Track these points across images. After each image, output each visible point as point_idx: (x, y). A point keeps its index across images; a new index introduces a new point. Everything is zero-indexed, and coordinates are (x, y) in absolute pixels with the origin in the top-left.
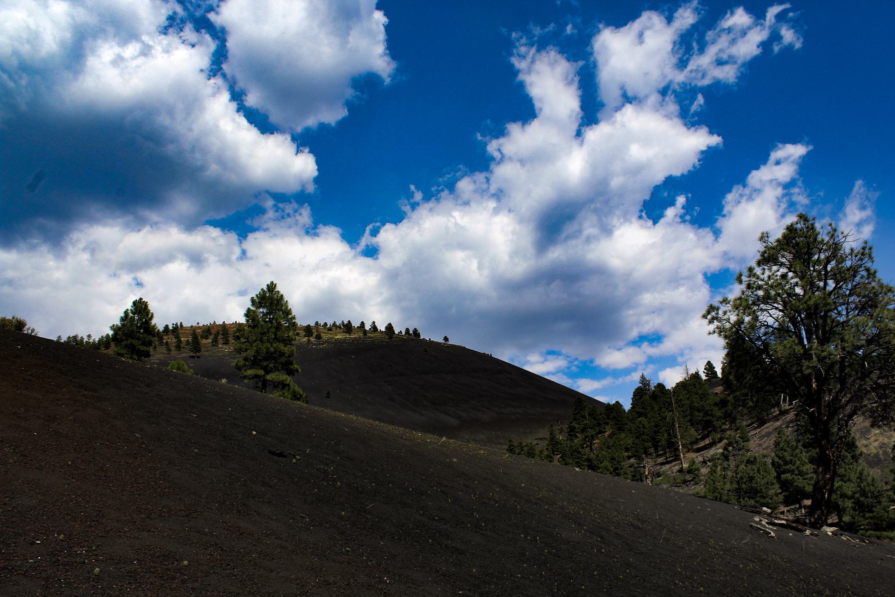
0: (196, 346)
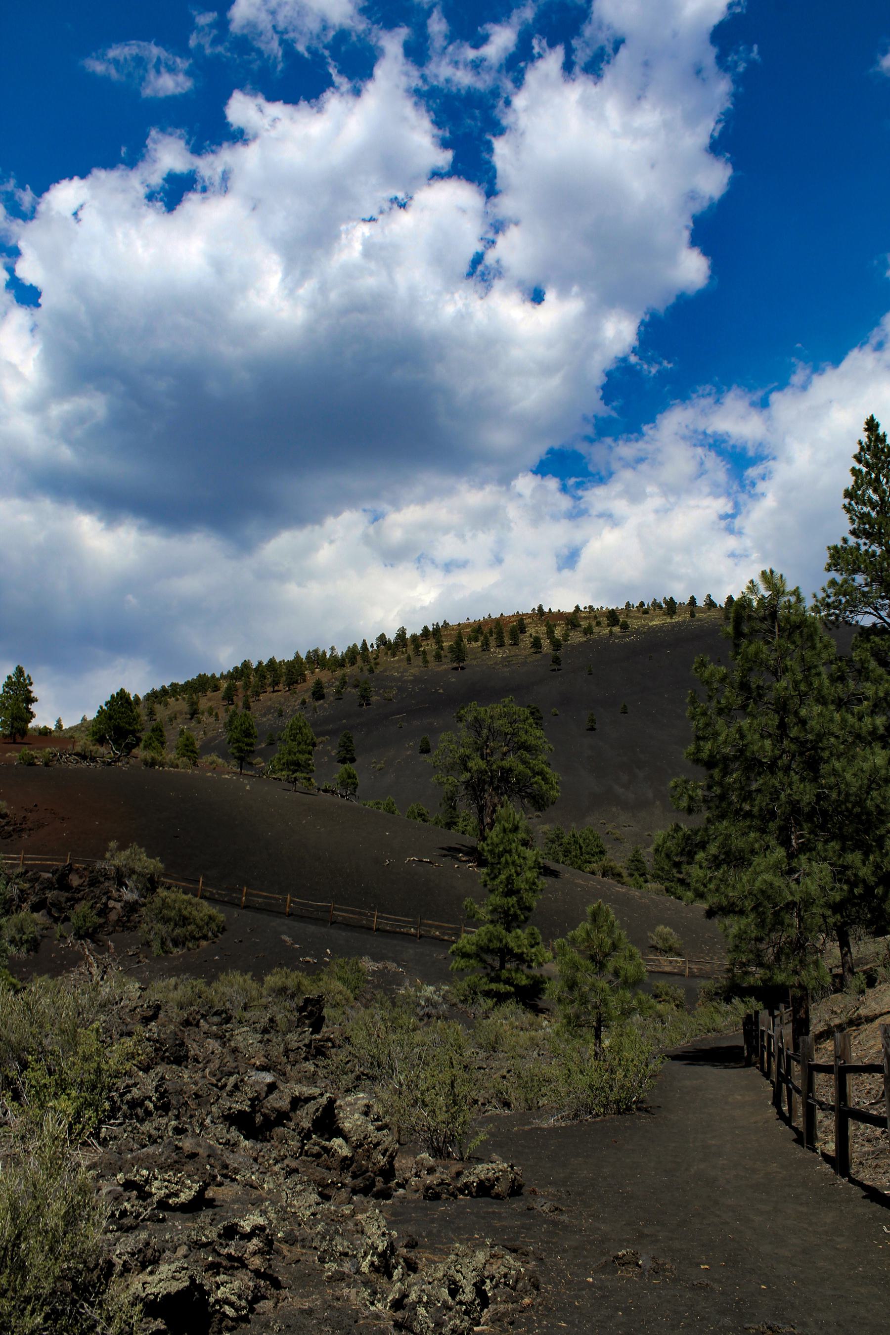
0: (458, 653)
